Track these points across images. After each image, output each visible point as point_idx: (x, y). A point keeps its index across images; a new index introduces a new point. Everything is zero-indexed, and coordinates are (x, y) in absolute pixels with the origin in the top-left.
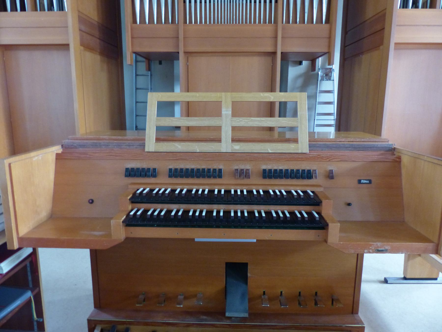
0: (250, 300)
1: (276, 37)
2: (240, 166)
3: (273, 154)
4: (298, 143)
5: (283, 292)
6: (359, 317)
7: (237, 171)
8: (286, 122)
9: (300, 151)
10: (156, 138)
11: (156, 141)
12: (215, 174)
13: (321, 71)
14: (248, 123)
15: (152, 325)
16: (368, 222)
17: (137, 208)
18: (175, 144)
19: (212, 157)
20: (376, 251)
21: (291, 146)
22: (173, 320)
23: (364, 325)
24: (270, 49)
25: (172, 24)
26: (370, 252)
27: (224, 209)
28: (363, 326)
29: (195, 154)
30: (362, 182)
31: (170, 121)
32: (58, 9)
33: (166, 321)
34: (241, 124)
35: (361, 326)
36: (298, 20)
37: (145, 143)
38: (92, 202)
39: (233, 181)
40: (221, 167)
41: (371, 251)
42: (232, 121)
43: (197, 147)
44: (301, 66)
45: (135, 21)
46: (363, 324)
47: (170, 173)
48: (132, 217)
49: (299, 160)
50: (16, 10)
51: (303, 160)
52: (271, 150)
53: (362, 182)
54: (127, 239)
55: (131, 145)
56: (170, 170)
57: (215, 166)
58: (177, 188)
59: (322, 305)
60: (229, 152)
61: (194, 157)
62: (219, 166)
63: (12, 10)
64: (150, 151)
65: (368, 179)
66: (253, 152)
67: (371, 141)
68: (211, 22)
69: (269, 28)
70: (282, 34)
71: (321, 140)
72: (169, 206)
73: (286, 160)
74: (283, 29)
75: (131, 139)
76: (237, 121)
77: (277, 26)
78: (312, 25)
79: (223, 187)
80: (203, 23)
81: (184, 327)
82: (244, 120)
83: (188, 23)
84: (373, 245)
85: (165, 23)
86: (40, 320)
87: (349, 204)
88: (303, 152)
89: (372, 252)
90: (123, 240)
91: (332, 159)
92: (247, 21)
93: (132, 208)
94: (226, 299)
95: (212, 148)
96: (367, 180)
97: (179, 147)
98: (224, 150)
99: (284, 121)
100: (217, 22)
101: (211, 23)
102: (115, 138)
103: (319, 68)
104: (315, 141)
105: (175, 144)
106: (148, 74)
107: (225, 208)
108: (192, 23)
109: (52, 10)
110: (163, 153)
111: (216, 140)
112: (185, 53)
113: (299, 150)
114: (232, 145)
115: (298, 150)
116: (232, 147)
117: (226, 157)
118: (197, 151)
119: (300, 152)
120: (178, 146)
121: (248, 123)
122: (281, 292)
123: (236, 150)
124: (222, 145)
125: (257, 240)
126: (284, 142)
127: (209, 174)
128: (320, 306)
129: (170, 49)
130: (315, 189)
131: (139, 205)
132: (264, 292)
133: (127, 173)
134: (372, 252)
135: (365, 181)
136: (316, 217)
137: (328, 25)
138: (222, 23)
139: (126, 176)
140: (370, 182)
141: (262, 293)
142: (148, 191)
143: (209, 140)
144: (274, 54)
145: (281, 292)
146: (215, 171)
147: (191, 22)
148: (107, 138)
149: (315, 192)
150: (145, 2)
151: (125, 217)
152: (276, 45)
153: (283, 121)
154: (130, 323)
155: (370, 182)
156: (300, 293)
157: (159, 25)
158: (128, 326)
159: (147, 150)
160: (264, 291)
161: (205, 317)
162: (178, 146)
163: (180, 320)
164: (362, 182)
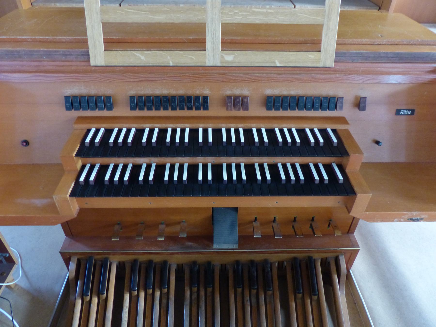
0: (240, 225)
2: (234, 90)
3: (283, 69)
4: (320, 51)
5: (277, 218)
6: (354, 237)
7: (230, 100)
8: (306, 17)
9: (321, 65)
10: (104, 39)
11: (106, 43)
12: (197, 105)
14: (248, 17)
15: (133, 255)
16: (397, 164)
17: (91, 163)
18: (135, 53)
19: (193, 77)
20: (409, 219)
21: (310, 56)
22: (155, 249)
23: (360, 248)
26: (400, 221)
27: (212, 162)
28: (358, 248)
29: (167, 68)
30: (401, 113)
31: (124, 13)
33: (148, 251)
34: (236, 18)
35: (356, 249)
37: (88, 52)
38: (26, 143)
39: (224, 113)
40: (206, 92)
41: (402, 220)
42: (222, 13)
43: (169, 58)
46: (359, 247)
47: (131, 104)
48: (83, 183)
49: (320, 81)
51: (325, 81)
52: (280, 63)
53: (402, 113)
54: (82, 211)
55: (69, 53)
56: (132, 98)
57: (198, 91)
58: (144, 127)
59: (319, 235)
60: (218, 65)
61: (166, 77)
62: (203, 91)
64: (99, 65)
65: (408, 108)
66: (252, 65)
71: (352, 43)
72: (135, 160)
73: (301, 81)
75: (67, 40)
76: (231, 15)
79: (210, 125)
81: (168, 255)
82: (241, 12)
84: (407, 214)
86: (6, 255)
87: (377, 143)
88: (326, 66)
89: (403, 221)
90: (76, 216)
91: (366, 81)
93: (82, 163)
94: (213, 224)
95: (192, 59)
96: (409, 110)
97: (143, 58)
98: (210, 62)
99: (303, 15)
102: (41, 39)
104: (344, 43)
105: (135, 53)
107: (213, 161)
110: (118, 67)
111: (198, 41)
113: (321, 63)
114: (224, 55)
115: (320, 62)
116: (222, 57)
117: (214, 77)
118: (170, 63)
119: (321, 66)
120: (140, 56)
121: (248, 17)
122: (275, 218)
123: (228, 62)
124: (207, 53)
127: (189, 104)
128: (317, 236)
130: (338, 127)
131: (92, 160)
132: (256, 219)
133: (67, 104)
134: (403, 221)
135: (406, 112)
136: (339, 179)
139: (68, 109)
140: (413, 111)
141: (254, 219)
142: (103, 136)
143: (186, 42)
145: (275, 218)
146: (198, 100)
148: (28, 39)
149: (338, 131)
151: (73, 185)
153: (301, 13)
154: (109, 254)
155: (413, 111)
156: (295, 218)
158: (107, 256)
159: (92, 63)
160: (256, 217)
161: (190, 244)
162: (140, 56)
163: (163, 249)
164: (402, 113)
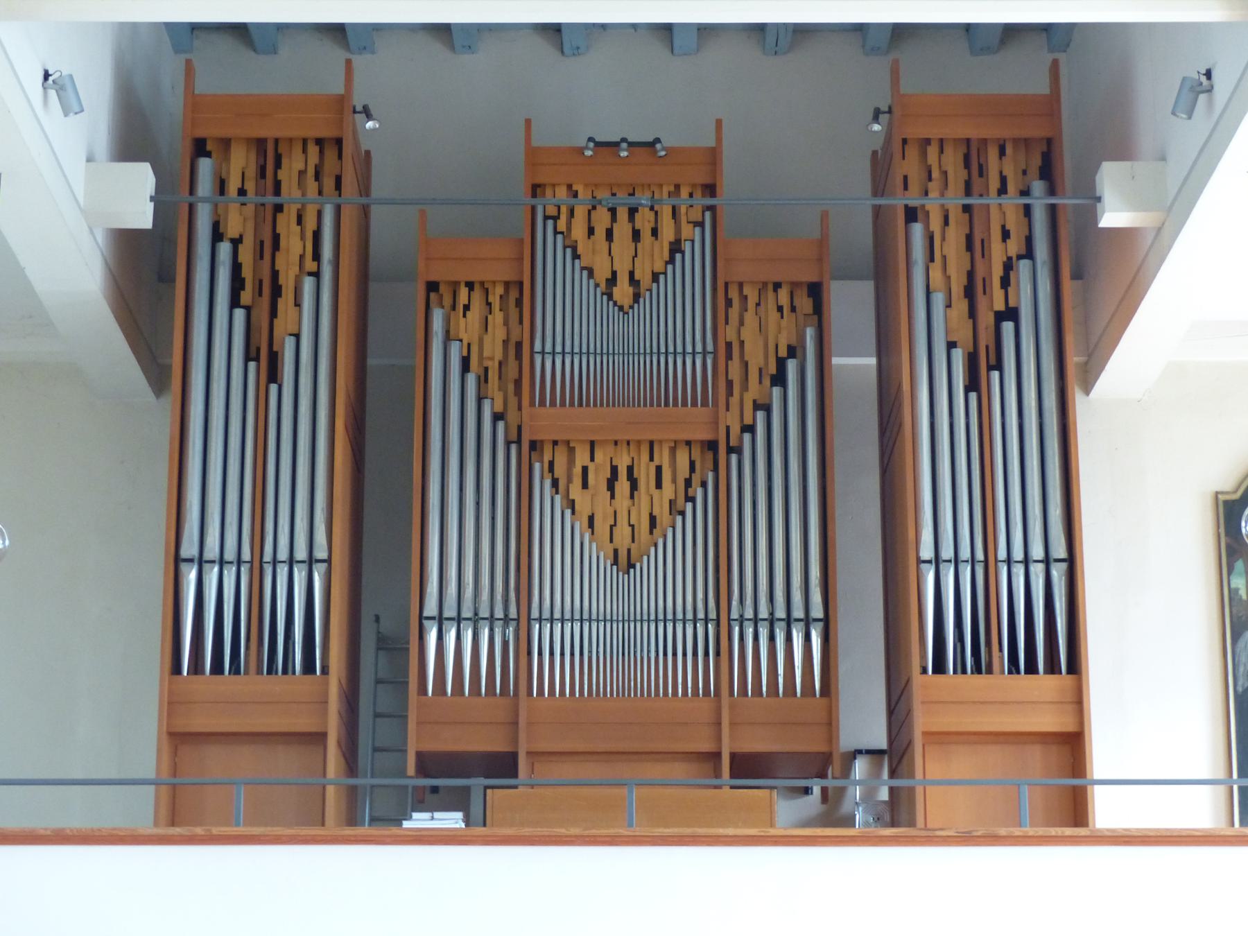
1: (719, 724)
13: (861, 809)
24: (706, 746)
25: (502, 697)
32: (164, 812)
36: (764, 689)
44: (810, 797)
45: (423, 689)
63: (1027, 672)
67: (550, 783)
68: (533, 694)
69: (705, 706)
74: (732, 707)
77: (719, 701)
80: (546, 696)
85: (501, 694)
92: (659, 691)
103: (856, 803)
109: (274, 673)
112: (529, 753)
125: (401, 825)
137: (825, 700)
144: (717, 755)
152: (719, 739)
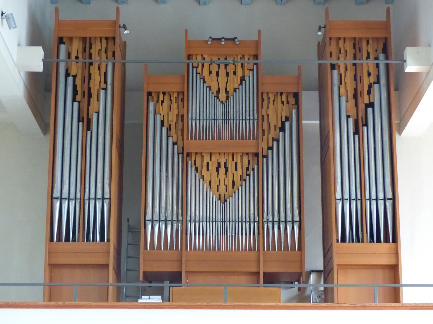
1: (259, 261)
24: (254, 270)
50: (84, 241)
70: (263, 259)
74: (264, 255)
77: (259, 252)
78: (288, 252)
83: (237, 250)
100: (228, 138)
101: (243, 250)
106: (139, 295)
108: (192, 250)
112: (186, 272)
126: (168, 173)
129: (175, 269)
137: (299, 252)
138: (218, 250)
144: (258, 273)
147: (191, 249)
150: (63, 206)
157: (166, 252)
